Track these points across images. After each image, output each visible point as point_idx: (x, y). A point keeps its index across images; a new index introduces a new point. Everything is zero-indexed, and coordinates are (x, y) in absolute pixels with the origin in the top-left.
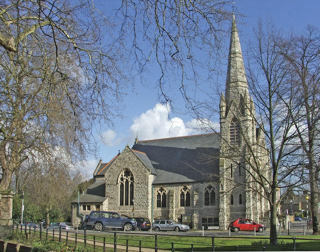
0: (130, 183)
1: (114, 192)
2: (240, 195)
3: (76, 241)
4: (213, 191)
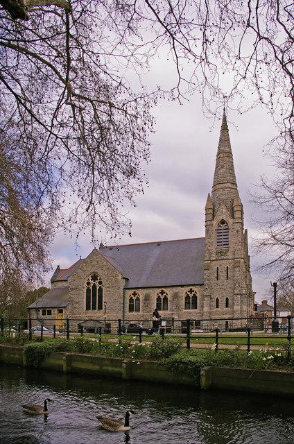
0: (98, 288)
2: (227, 299)
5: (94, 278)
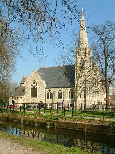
0: (35, 87)
1: (29, 92)
3: (34, 111)
4: (51, 92)
5: (34, 83)
